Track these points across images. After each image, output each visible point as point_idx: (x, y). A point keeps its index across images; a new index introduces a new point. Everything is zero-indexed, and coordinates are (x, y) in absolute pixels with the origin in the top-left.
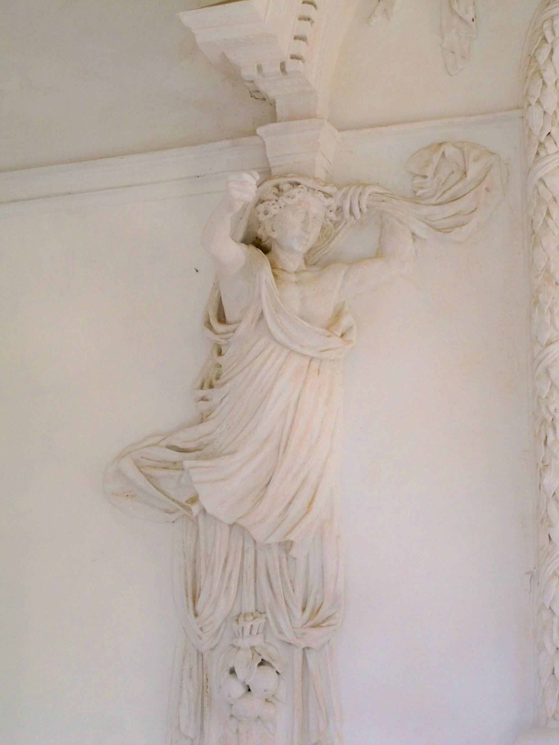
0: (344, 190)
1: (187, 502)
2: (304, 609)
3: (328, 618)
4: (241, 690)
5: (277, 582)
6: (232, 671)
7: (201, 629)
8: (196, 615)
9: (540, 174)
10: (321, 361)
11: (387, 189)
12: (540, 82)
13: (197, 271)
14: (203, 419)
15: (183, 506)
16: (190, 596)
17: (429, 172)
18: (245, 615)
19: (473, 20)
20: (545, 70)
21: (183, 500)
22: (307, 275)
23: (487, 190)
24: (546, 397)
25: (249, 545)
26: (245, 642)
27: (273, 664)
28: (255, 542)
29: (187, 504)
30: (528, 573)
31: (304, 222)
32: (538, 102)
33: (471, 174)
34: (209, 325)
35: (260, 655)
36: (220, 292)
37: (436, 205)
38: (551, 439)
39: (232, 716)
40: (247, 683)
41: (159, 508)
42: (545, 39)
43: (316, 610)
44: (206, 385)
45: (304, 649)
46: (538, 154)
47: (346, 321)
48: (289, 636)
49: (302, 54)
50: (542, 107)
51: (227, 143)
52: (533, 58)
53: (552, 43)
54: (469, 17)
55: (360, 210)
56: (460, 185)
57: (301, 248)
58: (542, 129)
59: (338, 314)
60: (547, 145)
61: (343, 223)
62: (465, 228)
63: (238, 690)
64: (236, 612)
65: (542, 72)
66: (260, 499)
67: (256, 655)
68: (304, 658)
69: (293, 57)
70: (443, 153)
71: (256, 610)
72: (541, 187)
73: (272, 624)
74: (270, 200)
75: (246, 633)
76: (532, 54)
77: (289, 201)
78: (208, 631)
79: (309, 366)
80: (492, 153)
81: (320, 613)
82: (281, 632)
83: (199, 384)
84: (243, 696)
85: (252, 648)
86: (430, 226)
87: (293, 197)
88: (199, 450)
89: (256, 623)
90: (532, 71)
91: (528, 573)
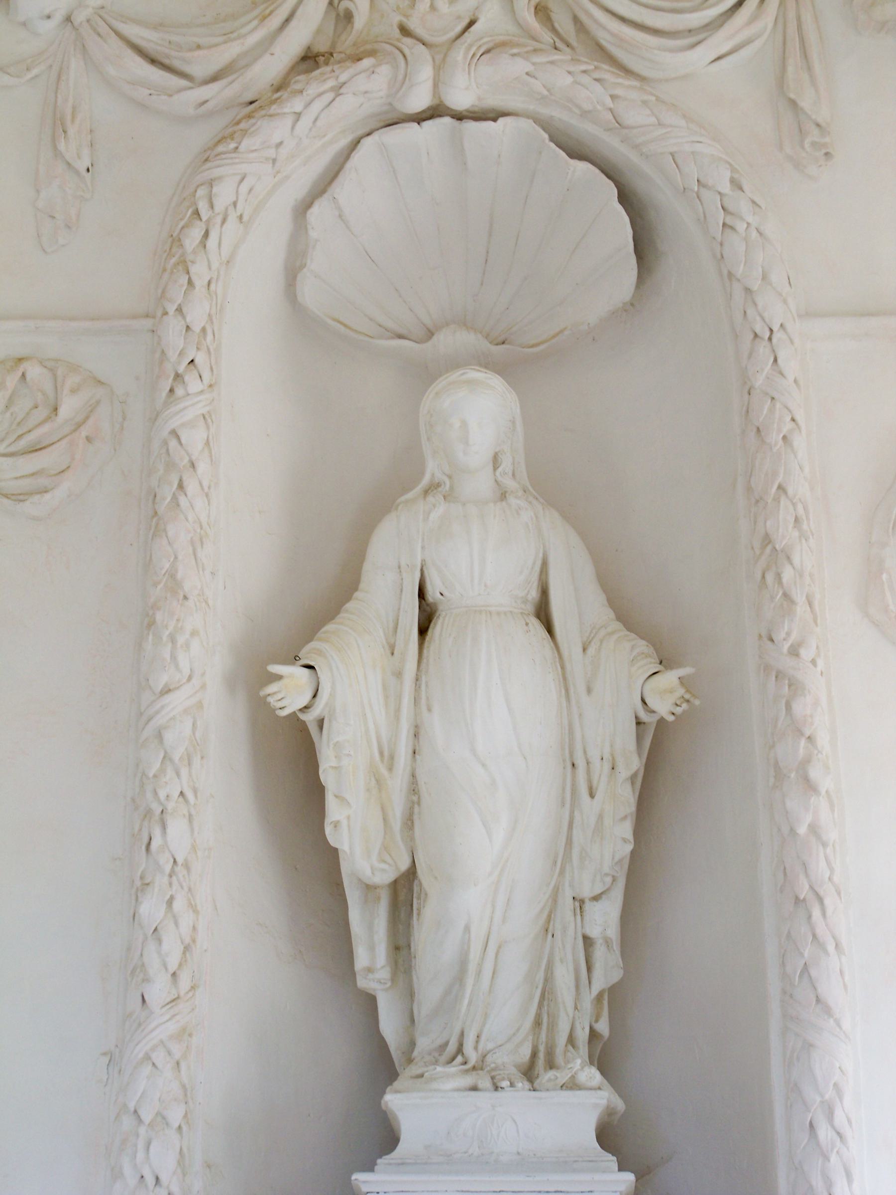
12: (184, 280)
19: (88, 170)
20: (193, 262)
23: (89, 439)
24: (155, 776)
30: (105, 1054)
32: (179, 310)
33: (65, 411)
42: (197, 213)
46: (171, 391)
50: (184, 317)
52: (176, 241)
53: (208, 221)
54: (82, 165)
58: (181, 354)
60: (187, 378)
62: (47, 496)
65: (189, 264)
70: (23, 375)
72: (173, 443)
90: (173, 260)
91: (105, 1054)
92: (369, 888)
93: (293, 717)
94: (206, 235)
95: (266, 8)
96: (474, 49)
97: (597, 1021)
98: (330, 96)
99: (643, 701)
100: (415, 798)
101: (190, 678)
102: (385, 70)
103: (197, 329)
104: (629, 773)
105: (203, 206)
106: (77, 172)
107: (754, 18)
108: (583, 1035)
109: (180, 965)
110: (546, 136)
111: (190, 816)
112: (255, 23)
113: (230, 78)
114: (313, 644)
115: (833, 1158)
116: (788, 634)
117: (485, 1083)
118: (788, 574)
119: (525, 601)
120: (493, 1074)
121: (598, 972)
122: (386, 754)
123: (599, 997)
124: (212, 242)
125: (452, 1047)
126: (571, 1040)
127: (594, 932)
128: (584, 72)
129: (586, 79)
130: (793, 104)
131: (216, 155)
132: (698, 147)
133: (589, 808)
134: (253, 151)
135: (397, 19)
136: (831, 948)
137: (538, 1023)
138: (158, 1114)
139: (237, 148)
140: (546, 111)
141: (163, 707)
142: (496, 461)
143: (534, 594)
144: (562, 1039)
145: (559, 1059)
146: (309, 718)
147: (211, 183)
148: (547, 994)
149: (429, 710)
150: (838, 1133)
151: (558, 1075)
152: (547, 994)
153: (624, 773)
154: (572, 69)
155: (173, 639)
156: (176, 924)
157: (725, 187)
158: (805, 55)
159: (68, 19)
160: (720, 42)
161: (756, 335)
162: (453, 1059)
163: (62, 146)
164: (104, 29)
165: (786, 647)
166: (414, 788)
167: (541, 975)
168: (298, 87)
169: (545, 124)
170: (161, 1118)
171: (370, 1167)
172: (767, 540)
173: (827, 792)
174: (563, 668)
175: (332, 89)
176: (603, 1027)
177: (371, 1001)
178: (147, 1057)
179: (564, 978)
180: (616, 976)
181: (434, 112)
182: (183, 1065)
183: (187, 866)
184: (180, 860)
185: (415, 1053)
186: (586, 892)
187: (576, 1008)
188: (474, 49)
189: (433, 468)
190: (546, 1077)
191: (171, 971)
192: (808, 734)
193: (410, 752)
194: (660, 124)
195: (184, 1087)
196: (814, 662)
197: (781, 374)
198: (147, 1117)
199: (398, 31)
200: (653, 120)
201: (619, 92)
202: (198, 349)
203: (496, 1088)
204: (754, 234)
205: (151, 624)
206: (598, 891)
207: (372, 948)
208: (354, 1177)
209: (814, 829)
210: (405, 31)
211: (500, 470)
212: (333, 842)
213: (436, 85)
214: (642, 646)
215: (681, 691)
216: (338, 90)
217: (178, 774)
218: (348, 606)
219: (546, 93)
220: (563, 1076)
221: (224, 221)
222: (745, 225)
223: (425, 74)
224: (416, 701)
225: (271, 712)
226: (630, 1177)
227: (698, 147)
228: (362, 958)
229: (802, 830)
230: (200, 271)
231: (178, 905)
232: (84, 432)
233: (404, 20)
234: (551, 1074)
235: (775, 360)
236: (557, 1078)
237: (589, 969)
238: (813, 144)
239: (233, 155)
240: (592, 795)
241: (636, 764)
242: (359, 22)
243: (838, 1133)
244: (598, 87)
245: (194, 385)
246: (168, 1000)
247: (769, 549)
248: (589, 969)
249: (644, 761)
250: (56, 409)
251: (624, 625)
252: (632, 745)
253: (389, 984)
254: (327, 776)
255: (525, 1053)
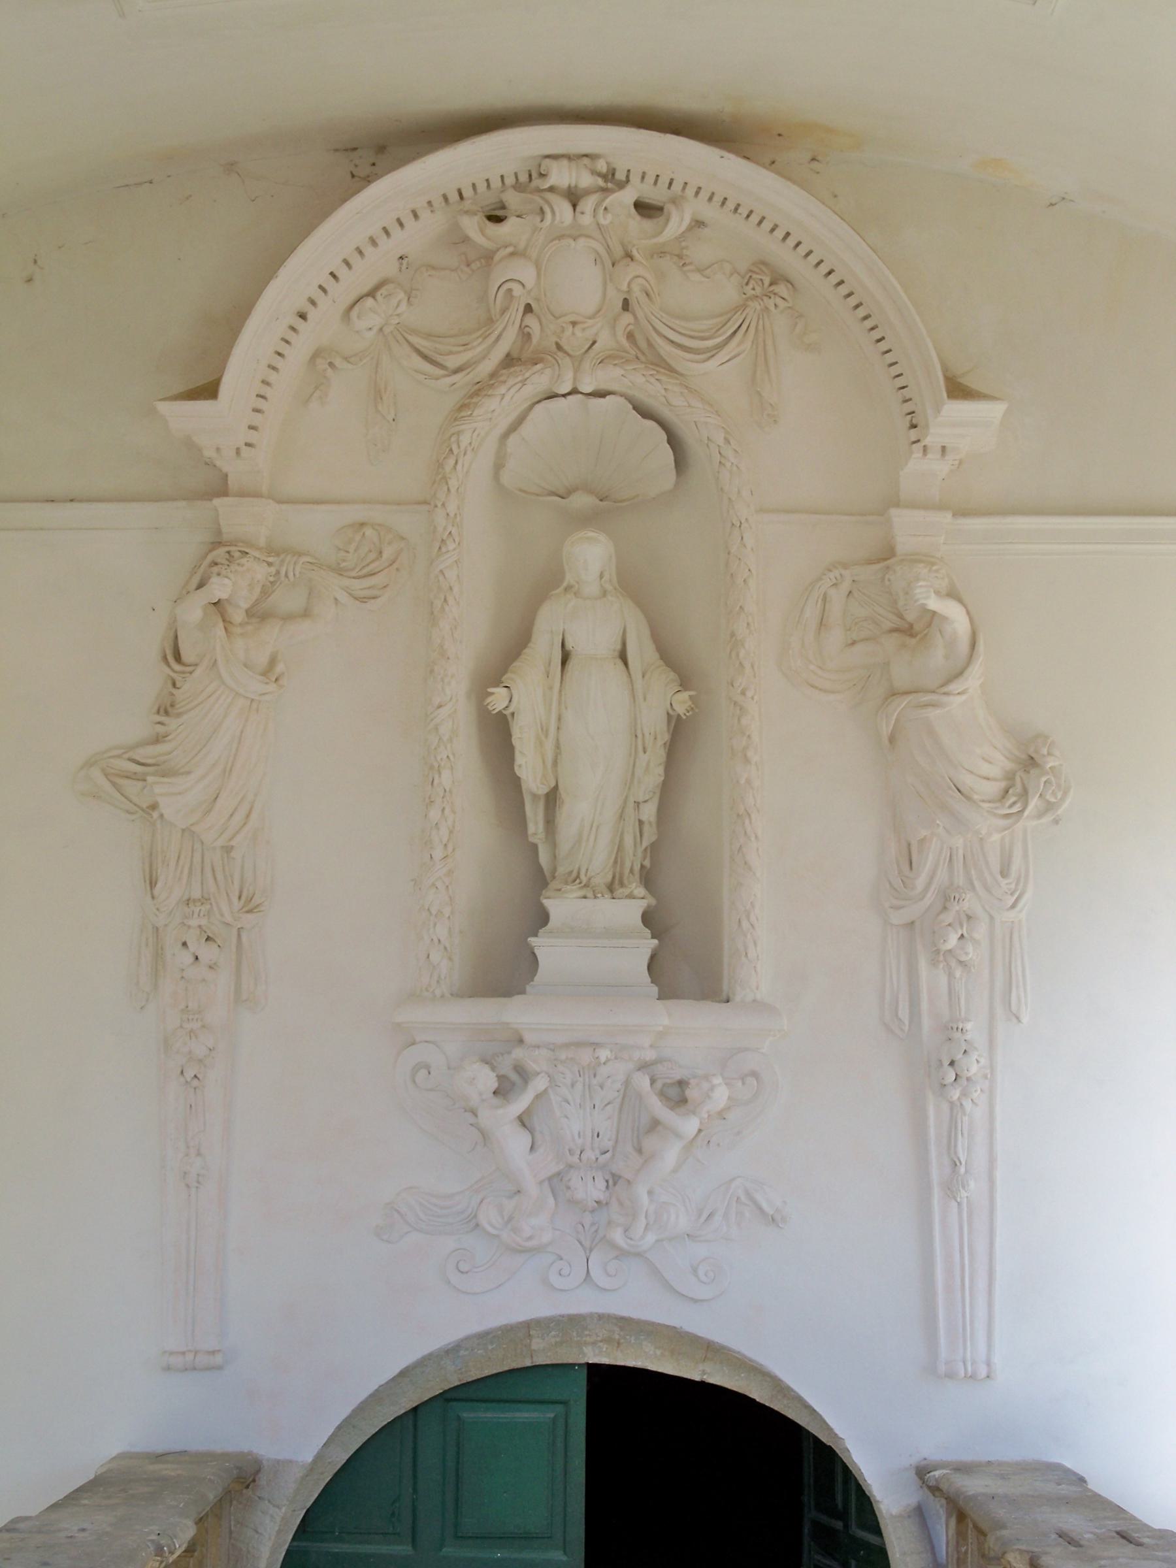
0: (282, 556)
1: (148, 807)
2: (240, 898)
3: (258, 905)
4: (192, 959)
5: (220, 877)
6: (184, 944)
7: (158, 909)
8: (153, 897)
9: (442, 567)
10: (260, 701)
11: (316, 559)
12: (445, 489)
13: (154, 610)
14: (158, 740)
15: (143, 810)
16: (148, 882)
17: (352, 551)
18: (194, 901)
19: (394, 420)
20: (450, 478)
21: (144, 806)
22: (250, 628)
23: (397, 569)
24: (435, 749)
25: (198, 846)
26: (194, 922)
27: (216, 940)
28: (202, 843)
29: (147, 810)
30: (412, 880)
31: (250, 585)
32: (443, 505)
33: (385, 555)
34: (165, 658)
35: (205, 932)
36: (176, 631)
37: (354, 578)
38: (436, 782)
39: (182, 977)
40: (197, 954)
41: (121, 809)
42: (451, 450)
43: (249, 899)
44: (162, 711)
45: (239, 928)
46: (440, 548)
47: (280, 668)
48: (228, 918)
49: (254, 441)
50: (446, 509)
51: (184, 503)
52: (440, 465)
53: (457, 455)
54: (390, 418)
55: (294, 575)
56: (377, 563)
57: (245, 605)
58: (445, 529)
59: (273, 662)
60: (448, 542)
61: (279, 583)
62: (378, 600)
63: (188, 958)
64: (186, 897)
65: (448, 480)
66: (208, 812)
67: (203, 933)
68: (239, 936)
69: (247, 444)
70: (364, 534)
71: (202, 897)
72: (441, 578)
73: (215, 909)
74: (222, 564)
75: (196, 915)
76: (440, 462)
77: (239, 569)
78: (1092, 1533)
79: (250, 706)
80: (403, 538)
81: (253, 901)
82: (222, 915)
83: (156, 708)
84: (192, 964)
85: (200, 927)
86: (350, 594)
87: (243, 566)
88: (158, 765)
89: (203, 908)
90: (440, 476)
91: (412, 880)
92: (535, 797)
93: (500, 712)
94: (456, 463)
95: (486, 331)
96: (594, 361)
97: (644, 861)
98: (520, 385)
99: (671, 704)
100: (559, 751)
101: (451, 699)
102: (548, 371)
103: (452, 515)
104: (663, 742)
105: (454, 447)
106: (388, 422)
107: (739, 345)
108: (637, 868)
109: (448, 841)
110: (631, 407)
111: (452, 766)
112: (480, 340)
113: (468, 370)
114: (508, 675)
115: (749, 936)
116: (741, 684)
117: (590, 894)
118: (742, 653)
119: (614, 650)
120: (594, 889)
121: (646, 835)
122: (545, 729)
123: (646, 849)
124: (459, 467)
125: (574, 874)
126: (632, 871)
127: (644, 818)
128: (651, 375)
129: (652, 380)
130: (759, 393)
131: (462, 417)
132: (709, 420)
133: (643, 758)
134: (480, 416)
135: (554, 339)
136: (753, 839)
137: (615, 862)
138: (439, 911)
139: (471, 414)
140: (630, 392)
141: (438, 714)
142: (601, 576)
143: (619, 647)
144: (627, 871)
145: (626, 882)
146: (507, 712)
147: (459, 433)
148: (620, 848)
149: (566, 708)
150: (752, 925)
151: (624, 890)
152: (620, 848)
153: (660, 743)
154: (645, 373)
155: (442, 680)
156: (446, 821)
157: (721, 442)
158: (766, 360)
159: (381, 329)
160: (723, 355)
161: (733, 524)
162: (575, 880)
163: (380, 408)
164: (400, 337)
165: (739, 691)
166: (558, 746)
167: (617, 841)
168: (502, 379)
169: (630, 400)
170: (440, 912)
171: (536, 935)
172: (733, 635)
173: (756, 763)
174: (632, 686)
175: (521, 381)
176: (647, 863)
177: (534, 847)
178: (433, 885)
179: (629, 840)
180: (654, 838)
181: (574, 392)
182: (450, 887)
183: (451, 792)
184: (448, 790)
185: (556, 874)
186: (641, 799)
187: (634, 855)
188: (594, 361)
189: (569, 578)
190: (620, 892)
191: (444, 843)
192: (748, 734)
193: (556, 728)
194: (689, 406)
195: (450, 897)
196: (752, 698)
197: (745, 546)
198: (434, 912)
199: (554, 346)
200: (686, 404)
201: (669, 387)
202: (453, 526)
203: (596, 897)
204: (735, 468)
205: (432, 671)
206: (646, 799)
207: (536, 823)
208: (529, 939)
209: (748, 781)
210: (559, 347)
211: (603, 580)
212: (518, 774)
213: (575, 379)
214: (672, 675)
215: (690, 703)
216: (524, 382)
217: (446, 748)
218: (525, 651)
219: (630, 384)
220: (626, 891)
221: (465, 454)
222: (730, 464)
223: (568, 376)
224: (560, 703)
225: (489, 712)
226: (656, 941)
227: (709, 420)
228: (531, 828)
229: (743, 781)
230: (453, 483)
231: (447, 811)
232: (395, 566)
233: (558, 340)
234: (621, 890)
235: (742, 538)
236: (623, 892)
237: (641, 836)
238: (768, 415)
239: (470, 418)
240: (645, 752)
241: (667, 737)
242: (535, 340)
243: (752, 925)
244: (658, 384)
245: (451, 546)
246: (443, 857)
247: (734, 638)
248: (641, 836)
249: (667, 750)
250: (381, 553)
251: (665, 662)
252: (665, 728)
253: (544, 840)
254: (515, 741)
255: (610, 877)
